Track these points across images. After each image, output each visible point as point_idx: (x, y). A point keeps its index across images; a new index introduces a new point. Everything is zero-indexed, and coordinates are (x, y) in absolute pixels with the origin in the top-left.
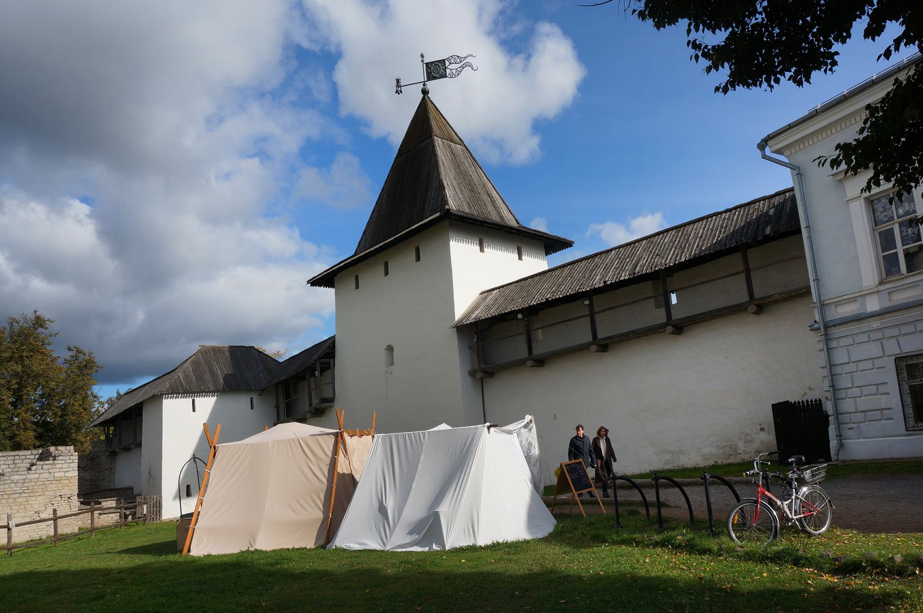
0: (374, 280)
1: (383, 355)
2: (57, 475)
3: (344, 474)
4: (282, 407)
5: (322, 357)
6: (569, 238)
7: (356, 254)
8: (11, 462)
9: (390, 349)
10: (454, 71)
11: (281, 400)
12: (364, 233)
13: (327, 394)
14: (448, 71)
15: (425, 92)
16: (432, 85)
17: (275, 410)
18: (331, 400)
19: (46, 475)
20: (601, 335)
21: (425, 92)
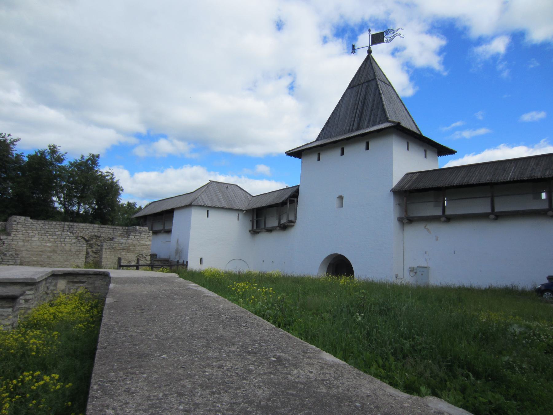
0: (331, 158)
1: (336, 202)
2: (142, 242)
3: (101, 262)
4: (255, 221)
5: (292, 197)
6: (454, 149)
7: (317, 140)
8: (112, 232)
9: (341, 198)
10: (389, 39)
11: (255, 218)
12: (323, 129)
13: (291, 218)
14: (385, 39)
15: (370, 52)
16: (373, 48)
17: (251, 223)
18: (293, 222)
19: (136, 242)
20: (497, 210)
21: (370, 52)
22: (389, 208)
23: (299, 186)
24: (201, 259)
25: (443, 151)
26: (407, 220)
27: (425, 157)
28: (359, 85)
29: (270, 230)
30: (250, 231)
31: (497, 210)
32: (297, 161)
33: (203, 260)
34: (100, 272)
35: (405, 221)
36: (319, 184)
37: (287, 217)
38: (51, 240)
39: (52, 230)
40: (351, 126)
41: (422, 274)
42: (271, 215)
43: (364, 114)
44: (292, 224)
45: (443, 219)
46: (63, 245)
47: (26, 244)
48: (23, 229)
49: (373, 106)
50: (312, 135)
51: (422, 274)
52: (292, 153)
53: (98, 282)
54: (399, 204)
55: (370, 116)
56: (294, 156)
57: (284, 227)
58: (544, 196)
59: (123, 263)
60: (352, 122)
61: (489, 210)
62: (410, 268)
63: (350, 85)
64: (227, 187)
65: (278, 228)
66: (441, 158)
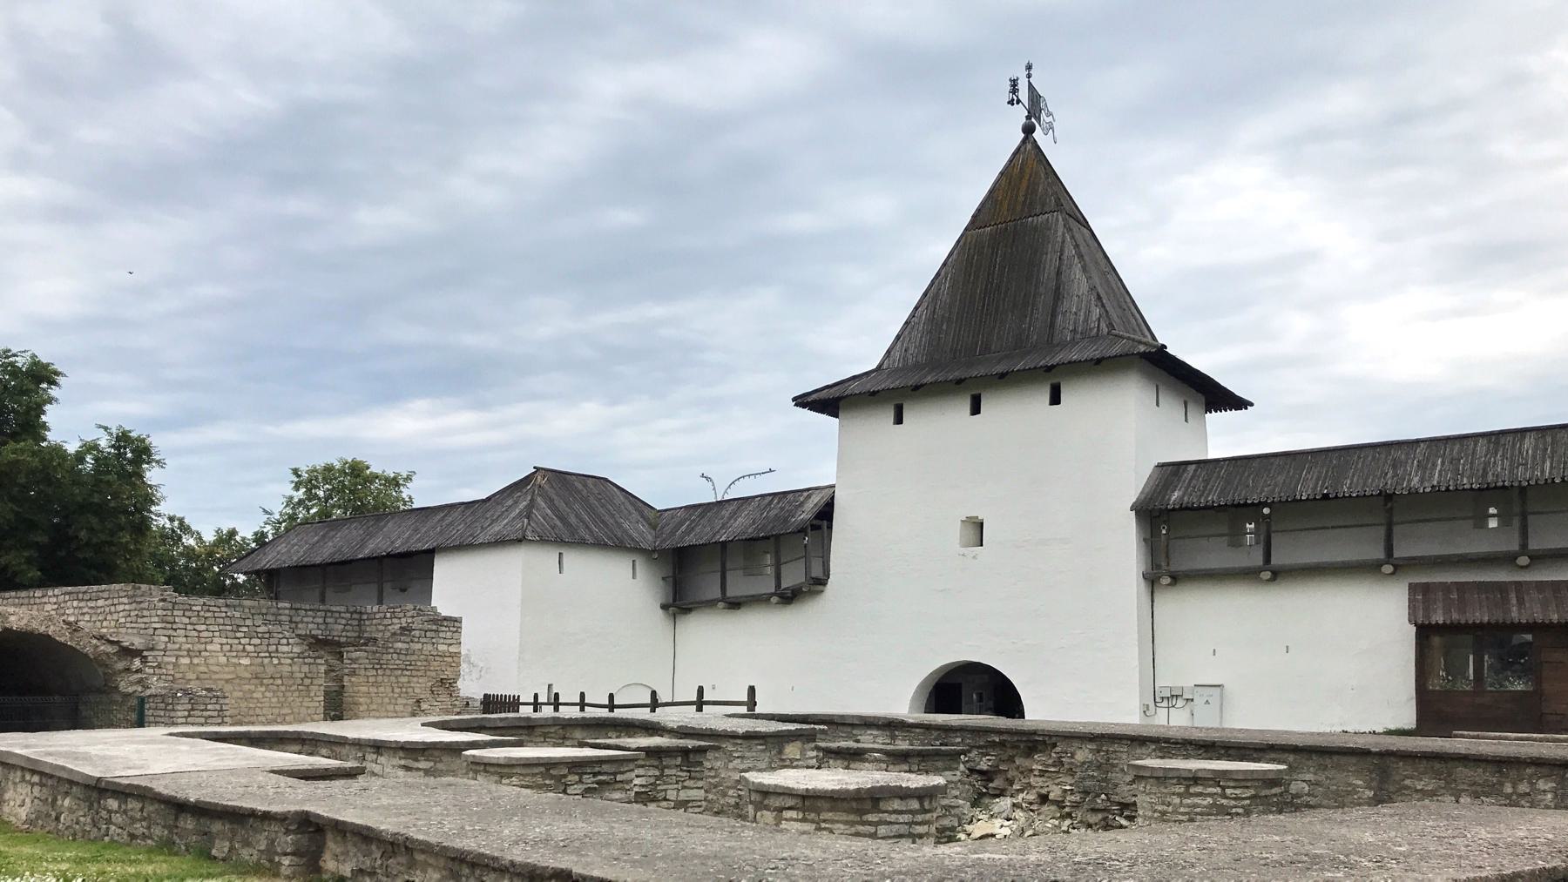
1: (955, 532)
13: (817, 572)
22: (1124, 547)
25: (1216, 397)
26: (1165, 570)
30: (664, 607)
31: (1533, 545)
34: (1199, 757)
36: (899, 489)
38: (249, 648)
39: (248, 622)
46: (275, 661)
47: (196, 661)
48: (186, 620)
52: (814, 402)
53: (134, 716)
57: (789, 597)
59: (663, 698)
61: (1515, 547)
65: (774, 599)
66: (1215, 419)
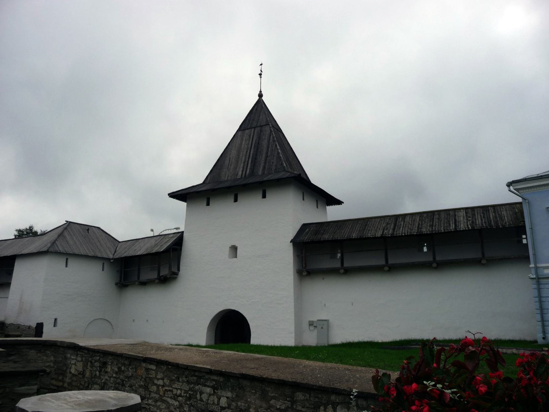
5: (175, 245)
9: (234, 249)
13: (174, 270)
18: (177, 274)
23: (183, 232)
24: (56, 320)
27: (317, 207)
28: (251, 128)
29: (144, 284)
30: (116, 284)
32: (182, 205)
33: (58, 321)
35: (305, 273)
37: (170, 268)
40: (244, 172)
41: (322, 328)
42: (151, 265)
43: (259, 159)
44: (175, 276)
45: (386, 268)
49: (267, 153)
50: (197, 176)
51: (322, 328)
54: (298, 256)
55: (265, 163)
56: (177, 199)
58: (425, 249)
60: (245, 167)
62: (310, 322)
63: (241, 126)
64: (88, 230)
65: (157, 281)
66: (330, 208)
